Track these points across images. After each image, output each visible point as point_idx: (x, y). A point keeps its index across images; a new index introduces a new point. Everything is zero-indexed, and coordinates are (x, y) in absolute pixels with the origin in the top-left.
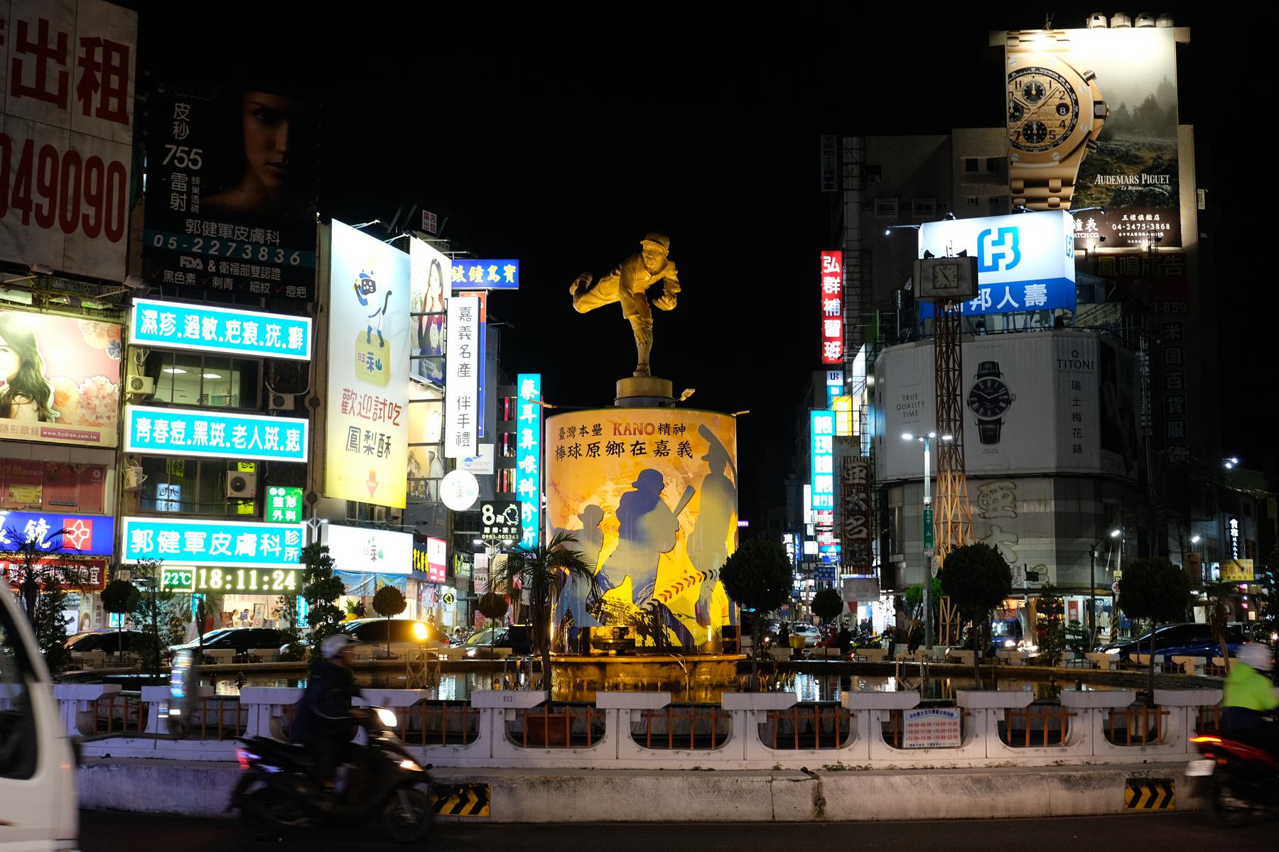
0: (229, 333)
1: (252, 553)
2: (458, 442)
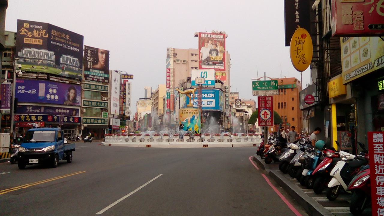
0: (97, 88)
1: (100, 123)
2: (128, 105)
